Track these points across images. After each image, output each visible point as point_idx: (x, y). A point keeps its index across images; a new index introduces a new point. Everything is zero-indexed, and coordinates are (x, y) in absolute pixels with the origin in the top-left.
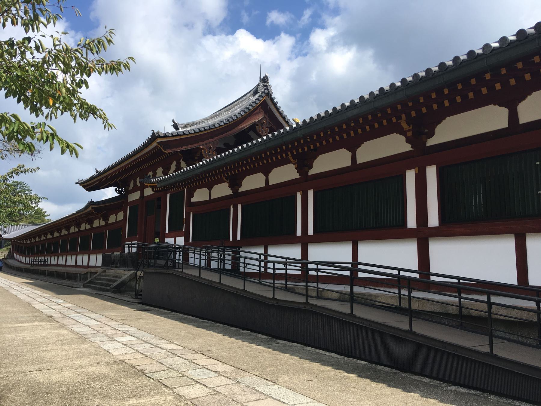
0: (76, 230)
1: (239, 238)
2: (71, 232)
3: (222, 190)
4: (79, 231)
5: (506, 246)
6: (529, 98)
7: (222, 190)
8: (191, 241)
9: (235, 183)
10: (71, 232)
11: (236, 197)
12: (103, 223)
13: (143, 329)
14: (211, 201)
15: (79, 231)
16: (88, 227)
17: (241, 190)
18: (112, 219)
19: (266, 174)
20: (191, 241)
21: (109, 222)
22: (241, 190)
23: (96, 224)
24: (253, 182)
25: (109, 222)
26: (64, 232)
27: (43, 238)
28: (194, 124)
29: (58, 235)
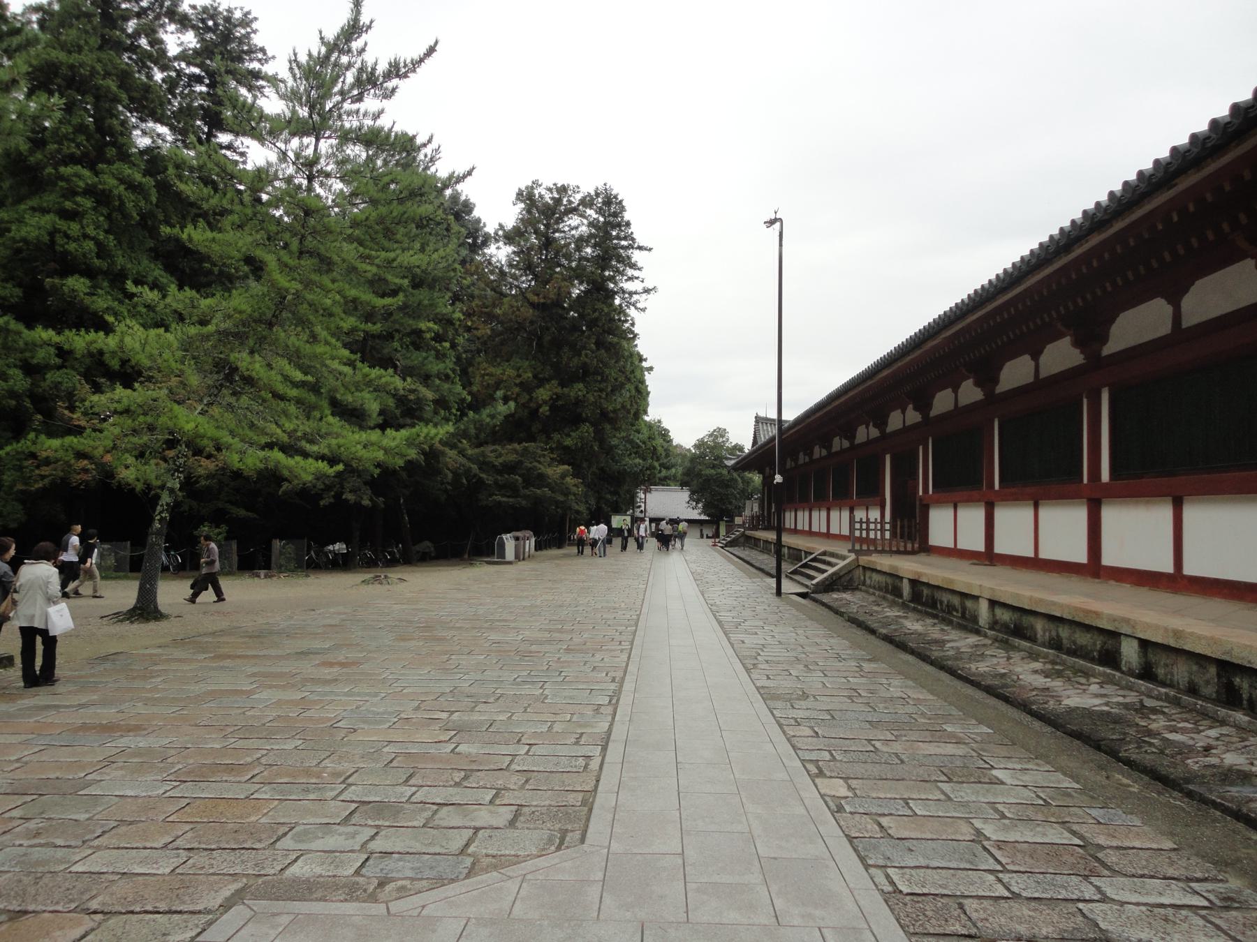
0: (846, 444)
1: (1105, 476)
2: (890, 429)
3: (1061, 355)
4: (853, 447)
5: (1162, 515)
6: (1192, 288)
7: (1061, 355)
8: (997, 486)
9: (987, 378)
10: (890, 429)
11: (1096, 367)
12: (874, 433)
13: (1170, 911)
14: (1180, 335)
15: (853, 447)
16: (874, 433)
17: (1109, 349)
18: (943, 402)
19: (1036, 356)
20: (997, 486)
21: (933, 413)
22: (1109, 349)
23: (895, 421)
24: (1016, 373)
25: (933, 413)
26: (838, 444)
27: (818, 452)
28: (557, 557)
29: (824, 452)
